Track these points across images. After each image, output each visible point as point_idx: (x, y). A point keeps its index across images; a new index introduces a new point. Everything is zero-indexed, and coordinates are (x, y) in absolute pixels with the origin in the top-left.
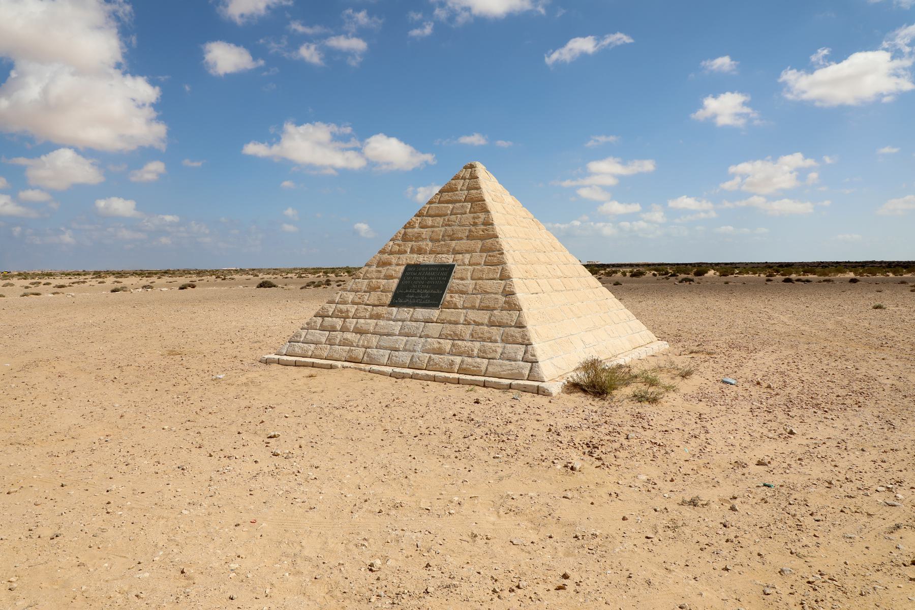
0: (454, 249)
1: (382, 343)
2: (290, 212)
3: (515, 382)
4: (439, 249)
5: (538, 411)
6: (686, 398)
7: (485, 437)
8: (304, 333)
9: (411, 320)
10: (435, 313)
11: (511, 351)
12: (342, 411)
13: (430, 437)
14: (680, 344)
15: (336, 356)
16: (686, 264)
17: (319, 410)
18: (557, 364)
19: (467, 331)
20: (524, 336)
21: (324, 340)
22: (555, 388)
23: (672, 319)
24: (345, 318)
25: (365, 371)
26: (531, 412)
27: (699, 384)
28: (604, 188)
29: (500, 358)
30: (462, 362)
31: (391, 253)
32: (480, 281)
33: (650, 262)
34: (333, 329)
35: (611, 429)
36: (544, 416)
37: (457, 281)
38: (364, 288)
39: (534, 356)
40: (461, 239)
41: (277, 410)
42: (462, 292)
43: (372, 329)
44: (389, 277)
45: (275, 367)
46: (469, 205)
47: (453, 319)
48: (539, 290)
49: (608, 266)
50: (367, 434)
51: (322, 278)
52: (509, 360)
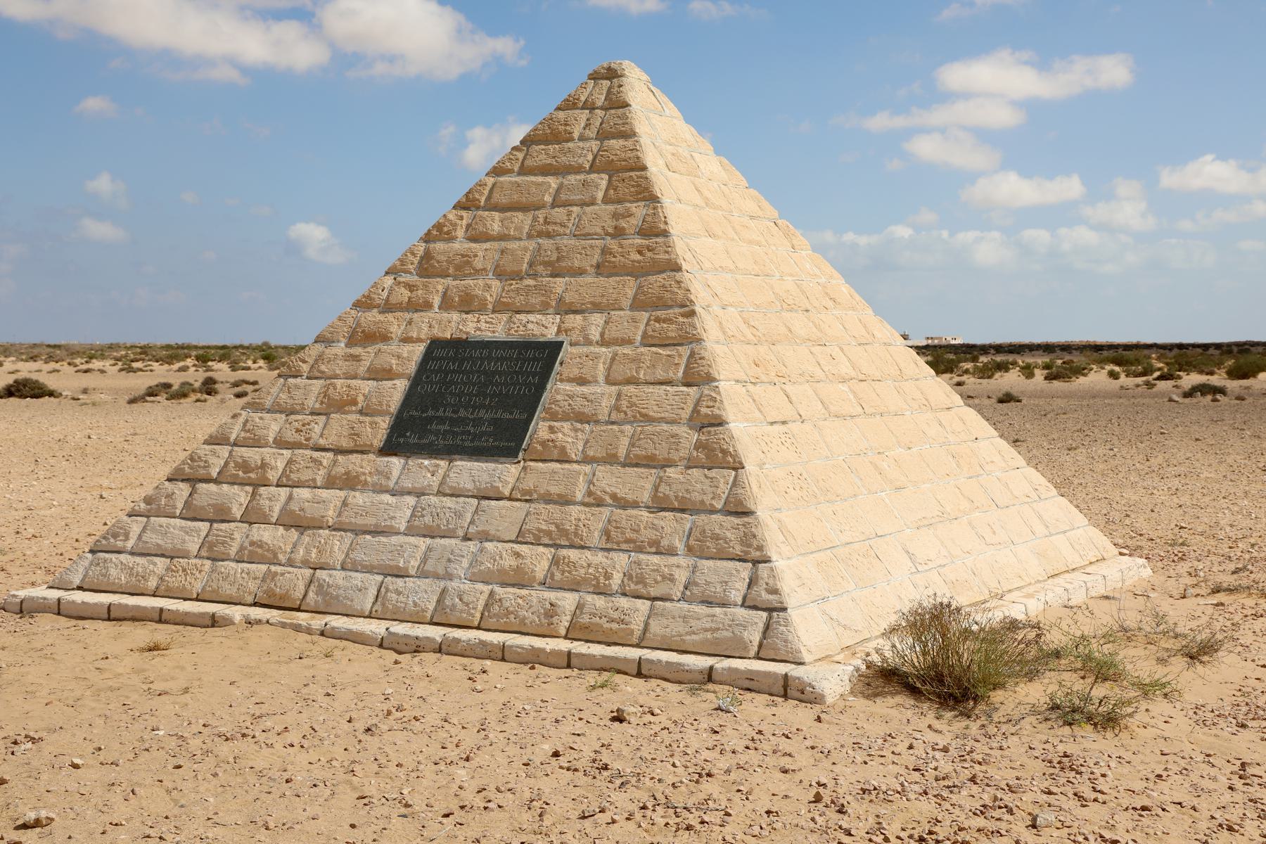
0: (560, 300)
1: (358, 556)
2: (103, 184)
3: (722, 664)
4: (519, 300)
5: (785, 745)
6: (1202, 717)
7: (638, 816)
8: (136, 526)
9: (440, 493)
10: (506, 473)
11: (713, 578)
12: (240, 745)
13: (487, 816)
14: (1184, 568)
15: (229, 590)
16: (1206, 347)
17: (173, 743)
18: (839, 616)
19: (594, 522)
20: (749, 538)
21: (193, 547)
22: (833, 681)
23: (1161, 496)
24: (256, 485)
25: (309, 631)
26: (766, 746)
27: (1238, 680)
28: (985, 136)
29: (683, 598)
30: (580, 606)
31: (388, 308)
32: (631, 389)
33: (1160, 341)
34: (221, 515)
35: (987, 799)
36: (803, 759)
37: (568, 387)
38: (311, 402)
39: (775, 591)
40: (581, 272)
41: (48, 748)
42: (582, 418)
43: (331, 515)
44: (381, 374)
45: (46, 622)
46: (602, 181)
47: (554, 490)
48: (788, 412)
49: (985, 349)
50: (311, 811)
51: (193, 369)
52: (708, 602)
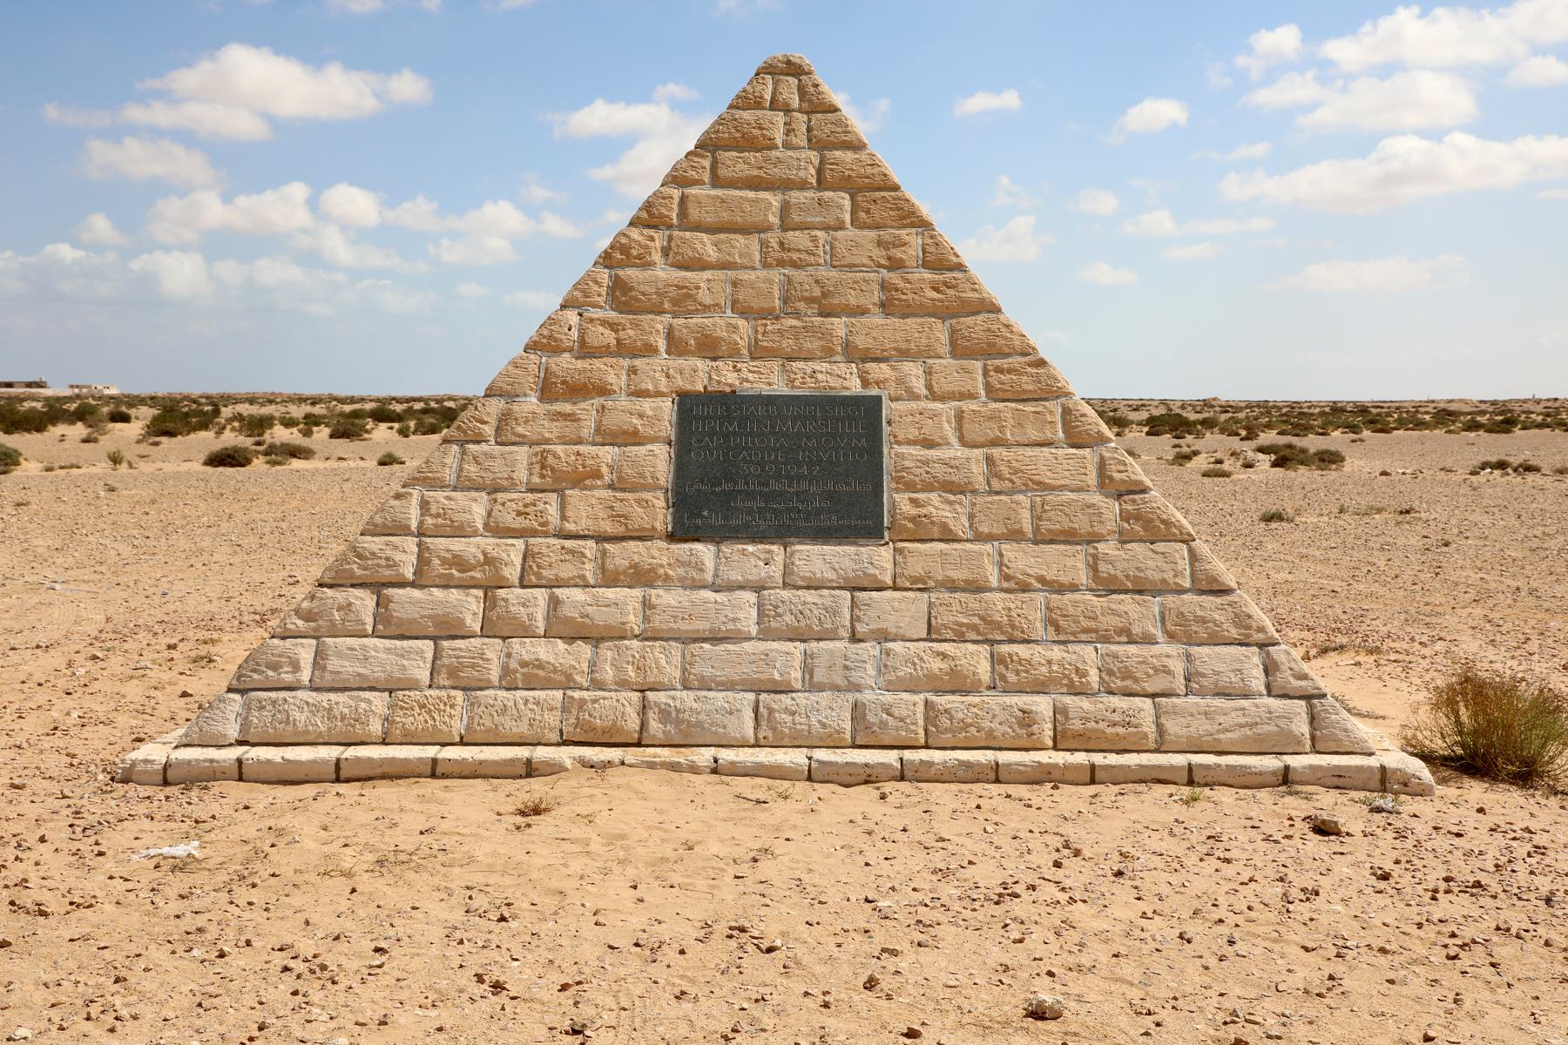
1: (702, 669)
19: (1032, 610)
40: (862, 311)
47: (958, 575)
